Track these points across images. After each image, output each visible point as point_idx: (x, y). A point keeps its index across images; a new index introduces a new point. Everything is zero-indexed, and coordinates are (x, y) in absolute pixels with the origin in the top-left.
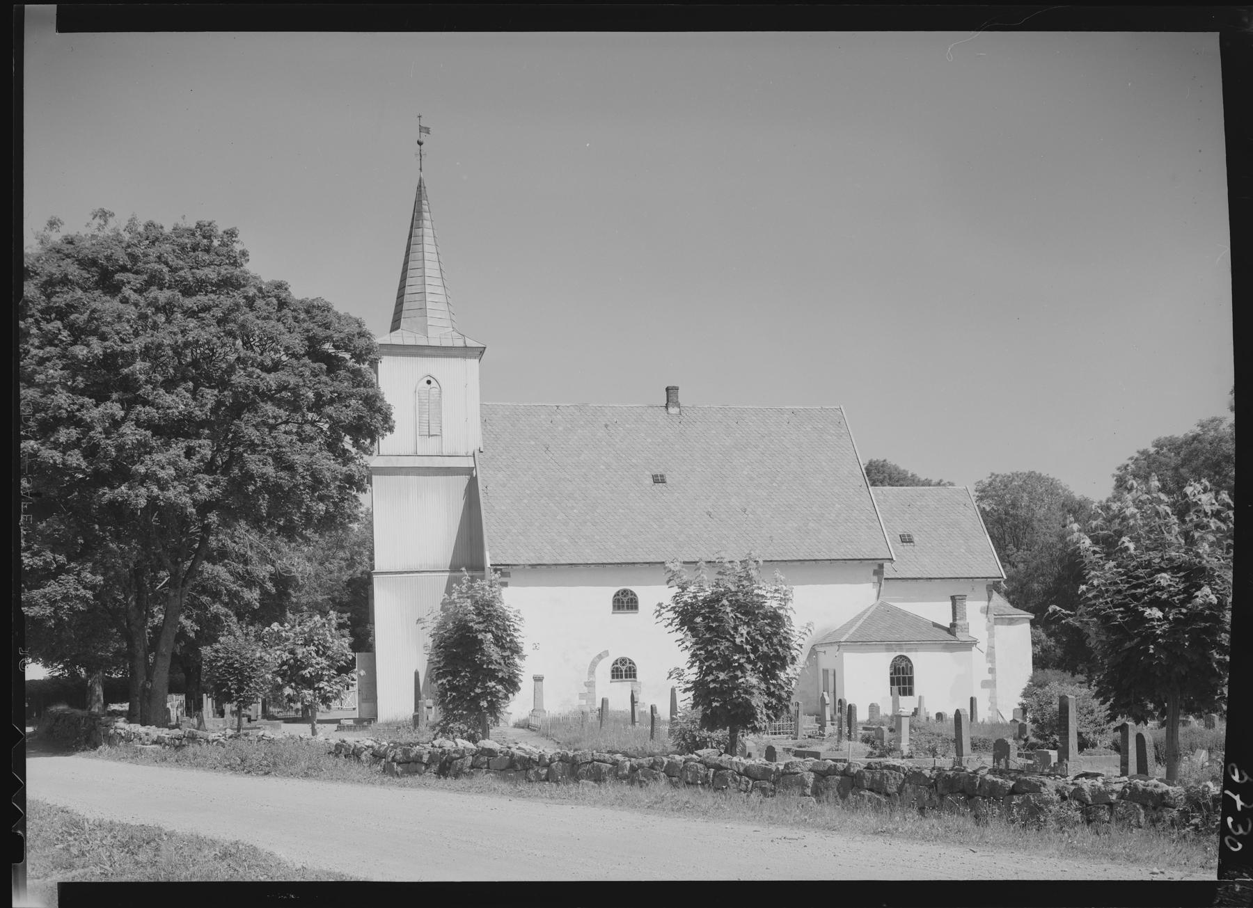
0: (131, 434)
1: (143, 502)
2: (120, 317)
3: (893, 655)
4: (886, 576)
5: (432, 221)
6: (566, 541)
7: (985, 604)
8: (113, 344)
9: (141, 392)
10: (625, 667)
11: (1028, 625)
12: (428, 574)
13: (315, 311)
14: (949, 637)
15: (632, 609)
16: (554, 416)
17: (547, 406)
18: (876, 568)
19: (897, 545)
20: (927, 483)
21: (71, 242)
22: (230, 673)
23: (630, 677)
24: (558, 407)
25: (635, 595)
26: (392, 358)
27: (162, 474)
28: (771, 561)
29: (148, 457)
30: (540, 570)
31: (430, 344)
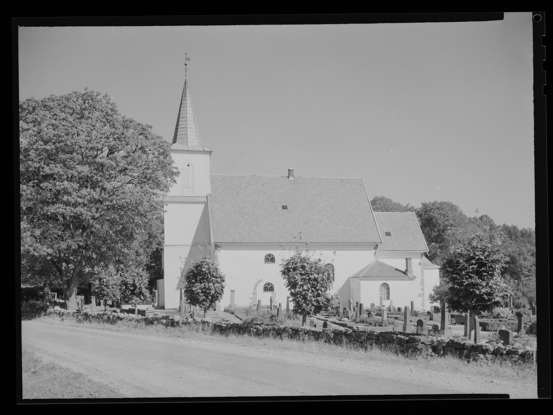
24: (243, 176)
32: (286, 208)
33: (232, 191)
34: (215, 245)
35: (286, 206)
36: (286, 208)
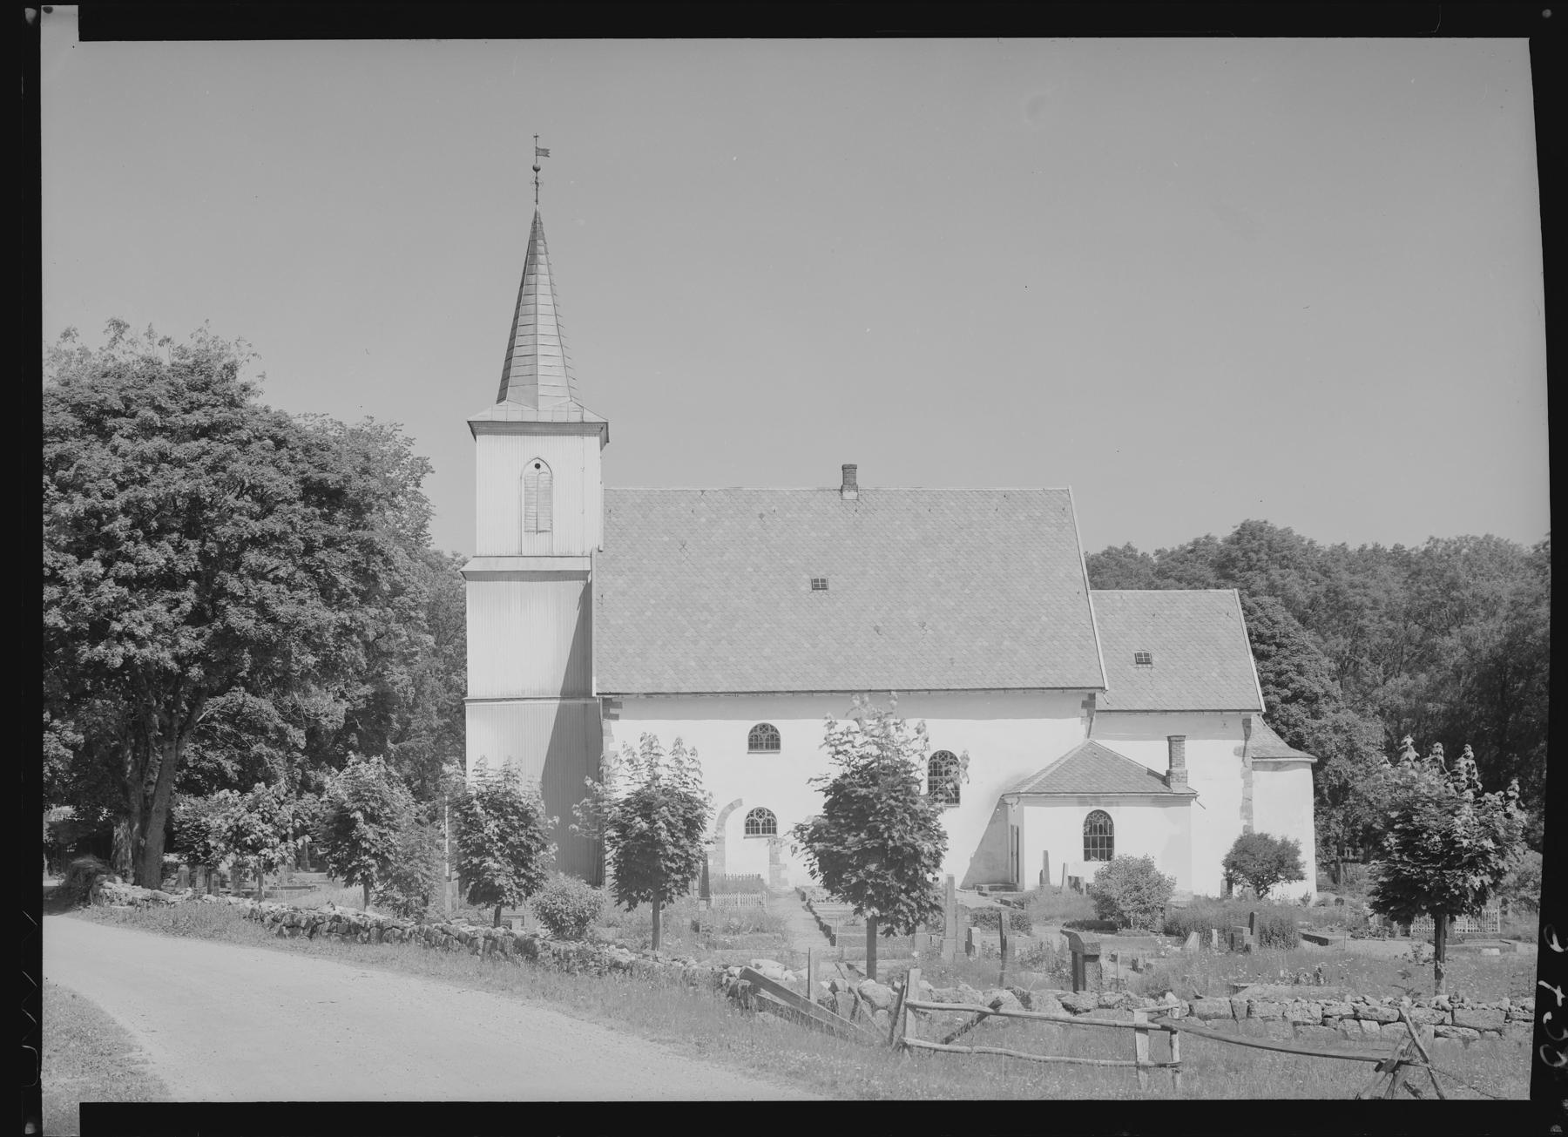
0: (109, 591)
1: (118, 662)
2: (105, 471)
3: (1086, 811)
4: (1097, 708)
5: (549, 264)
6: (693, 664)
7: (1241, 743)
8: (96, 501)
9: (123, 548)
10: (762, 820)
11: (1309, 772)
12: (532, 702)
13: (315, 450)
14: (1160, 787)
15: (773, 748)
17: (689, 491)
18: (1086, 698)
19: (1129, 666)
21: (67, 384)
22: (197, 836)
23: (769, 832)
24: (703, 491)
25: (776, 731)
26: (492, 438)
27: (139, 632)
28: (948, 690)
29: (126, 614)
30: (657, 700)
31: (540, 420)
32: (824, 588)
33: (666, 539)
34: (604, 699)
35: (823, 580)
36: (824, 588)
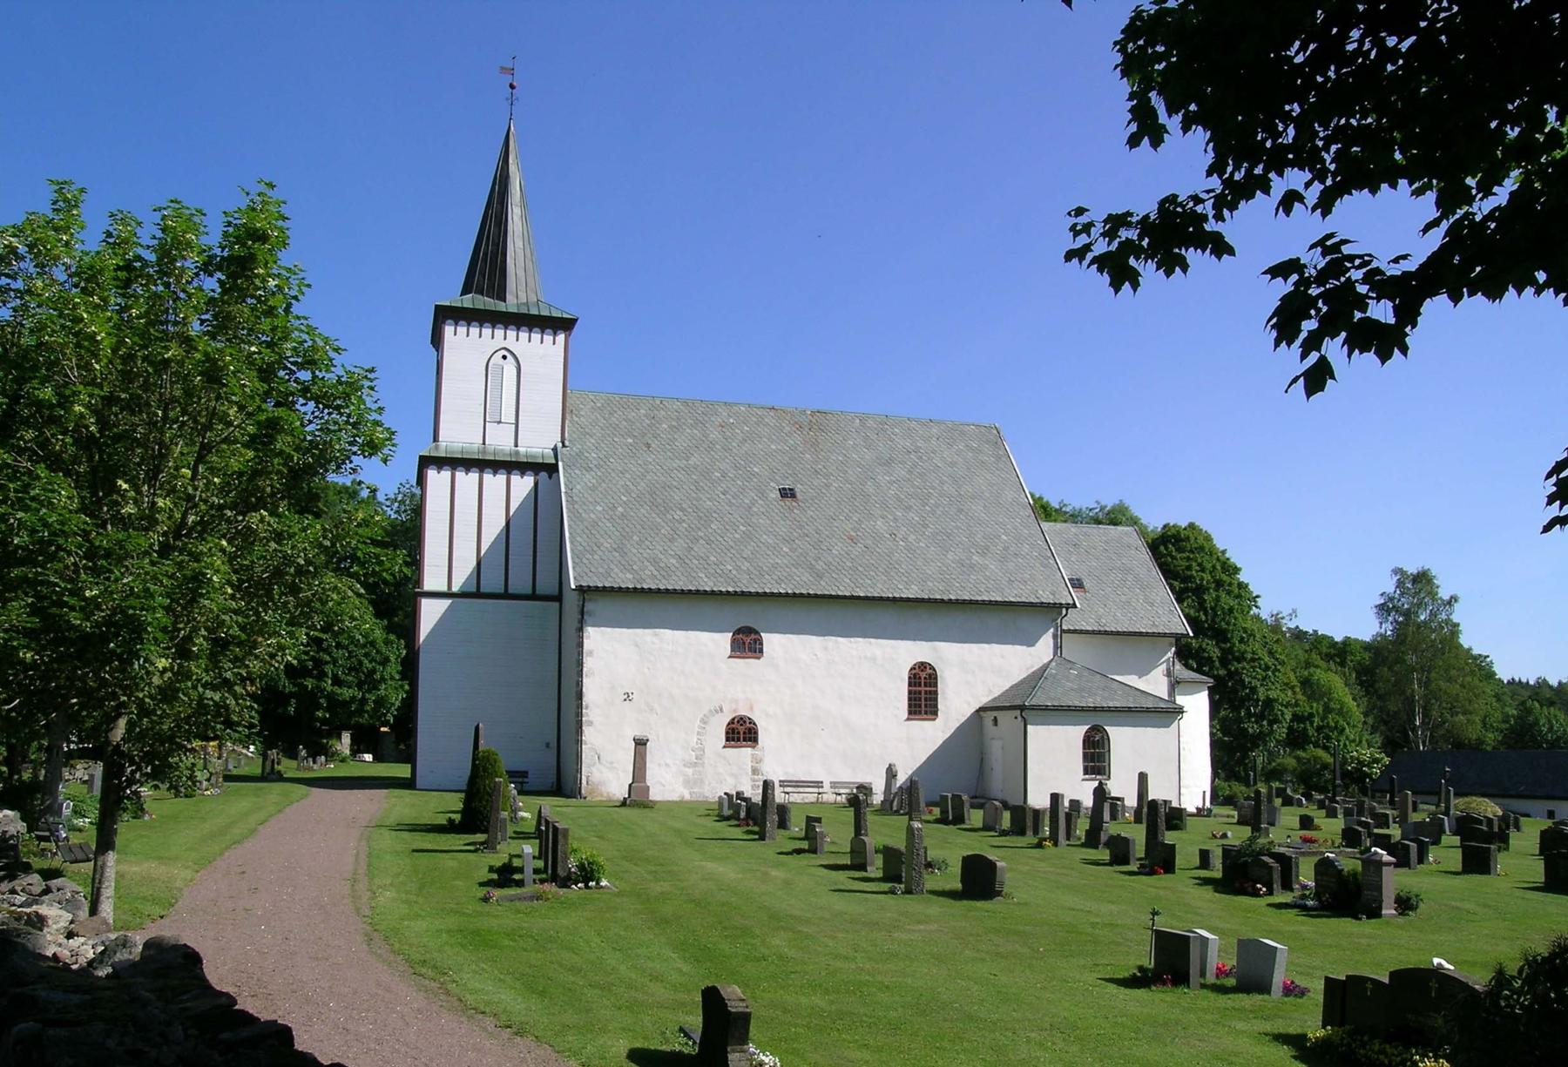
16: (656, 412)
20: (1289, 386)
